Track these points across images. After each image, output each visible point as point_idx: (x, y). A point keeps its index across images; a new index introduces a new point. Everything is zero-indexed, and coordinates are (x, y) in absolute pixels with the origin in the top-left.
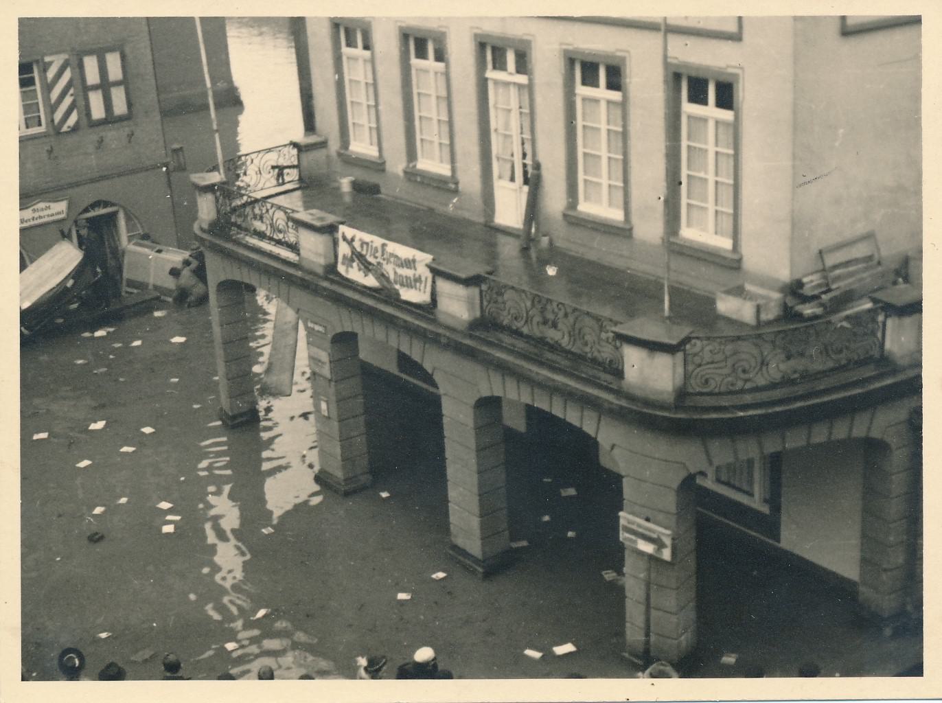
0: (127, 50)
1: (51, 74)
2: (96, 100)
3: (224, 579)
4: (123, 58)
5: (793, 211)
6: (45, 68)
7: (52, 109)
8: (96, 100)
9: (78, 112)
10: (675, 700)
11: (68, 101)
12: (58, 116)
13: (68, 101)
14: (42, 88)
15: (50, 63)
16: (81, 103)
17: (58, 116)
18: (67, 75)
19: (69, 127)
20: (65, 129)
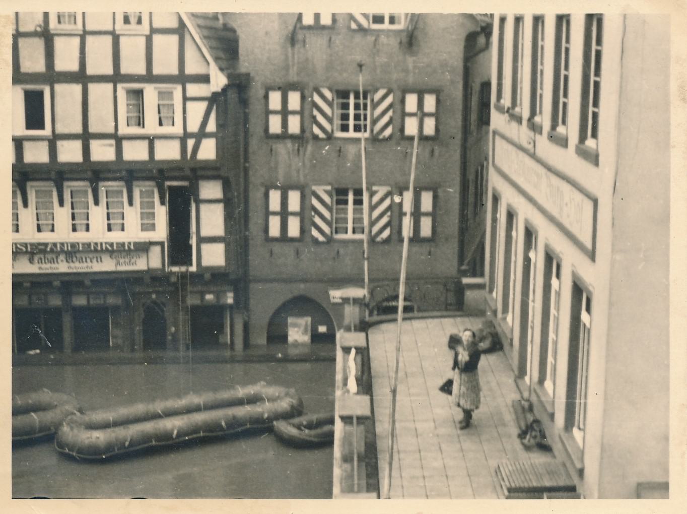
0: (440, 193)
1: (376, 199)
2: (407, 222)
3: (293, 77)
4: (435, 198)
5: (603, 437)
6: (372, 194)
7: (372, 224)
8: (407, 222)
9: (393, 127)
10: (57, 118)
11: (386, 119)
12: (375, 229)
13: (385, 220)
14: (367, 208)
15: (376, 192)
16: (397, 122)
17: (375, 229)
18: (389, 100)
19: (382, 238)
20: (379, 239)
